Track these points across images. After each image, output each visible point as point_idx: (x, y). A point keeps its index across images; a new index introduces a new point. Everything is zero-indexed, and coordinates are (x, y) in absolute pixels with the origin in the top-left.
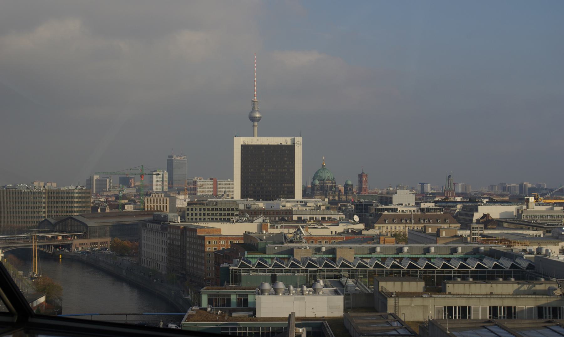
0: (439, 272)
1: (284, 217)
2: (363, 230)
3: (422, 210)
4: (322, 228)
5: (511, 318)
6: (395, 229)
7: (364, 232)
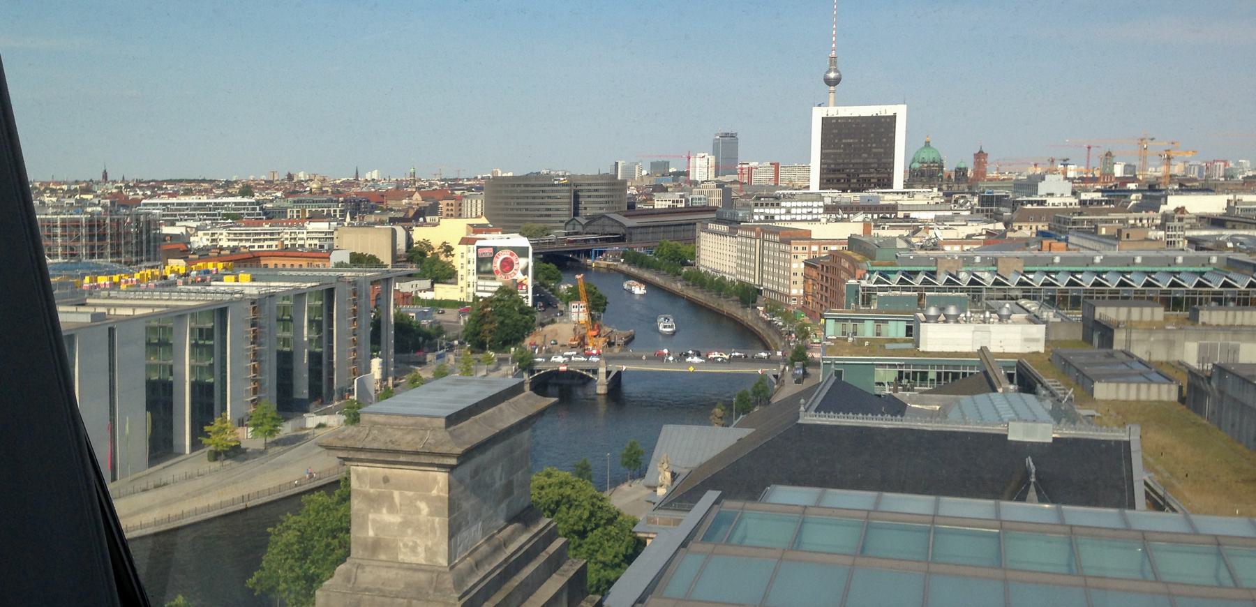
0: (1061, 291)
1: (887, 213)
3: (1083, 203)
5: (590, 379)
7: (1010, 234)
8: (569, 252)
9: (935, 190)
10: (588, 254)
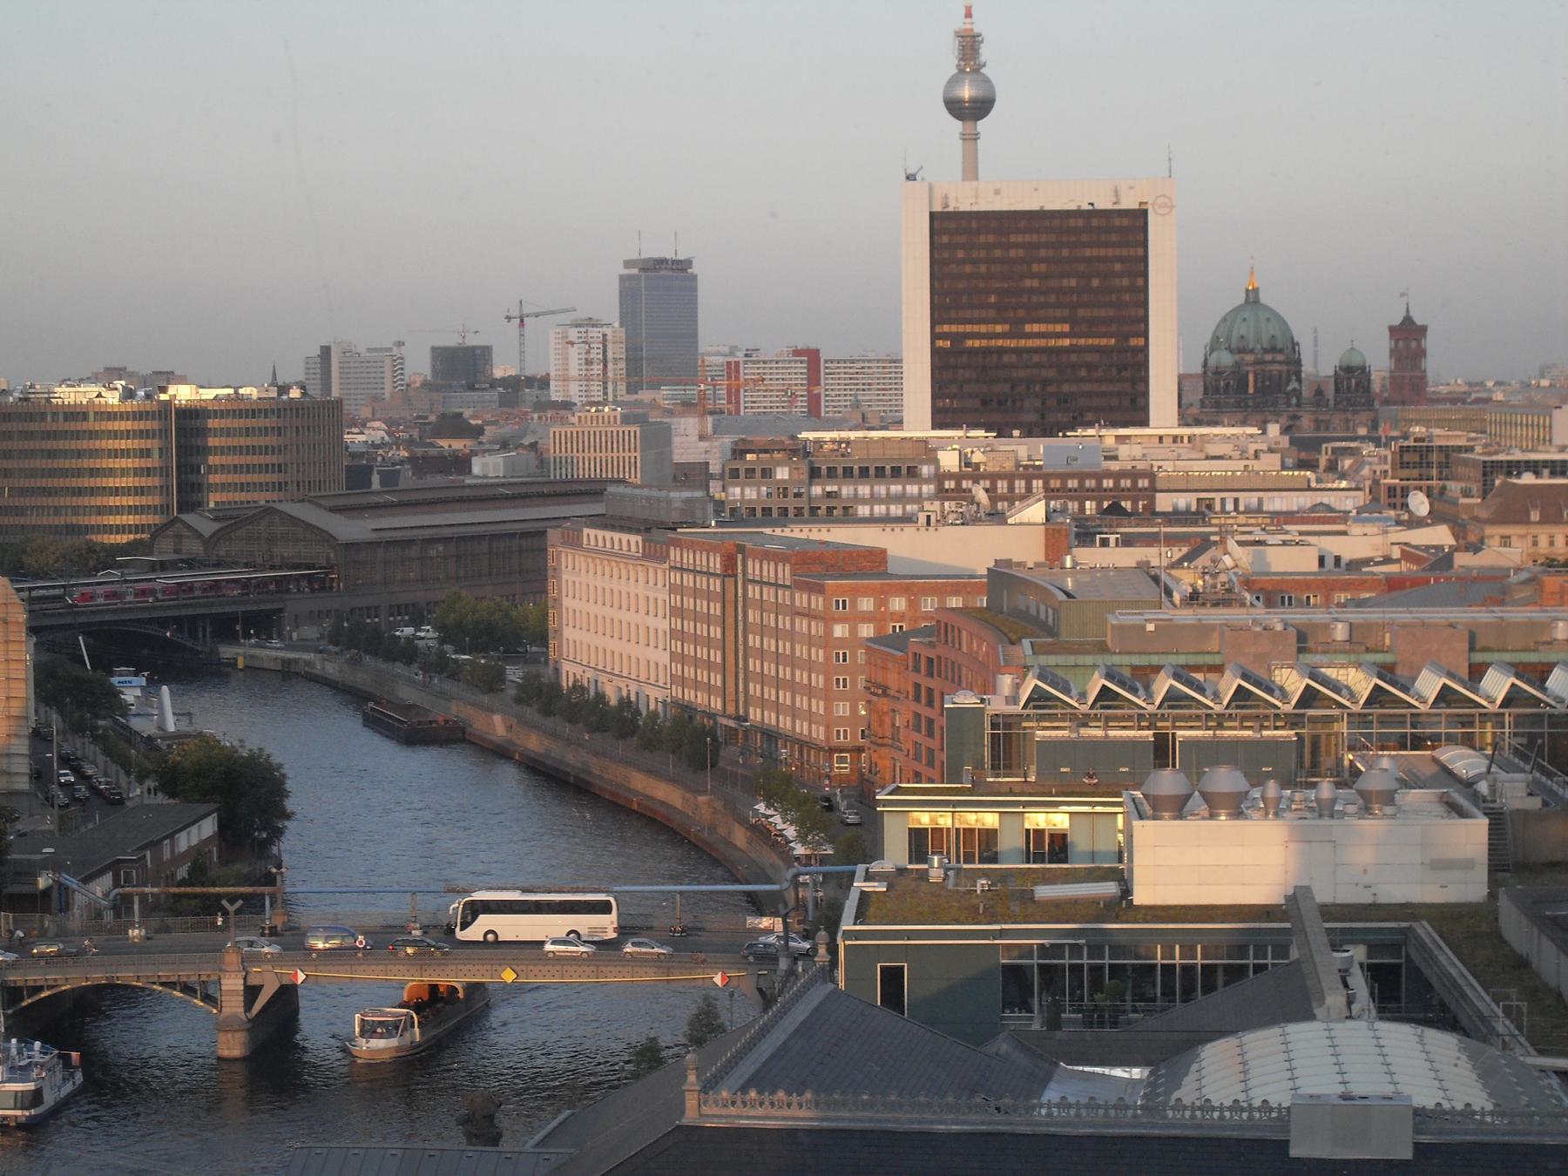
1: (1120, 505)
2: (1454, 549)
4: (1285, 543)
6: (1552, 543)
7: (1462, 560)
8: (163, 623)
9: (1274, 429)
10: (226, 628)
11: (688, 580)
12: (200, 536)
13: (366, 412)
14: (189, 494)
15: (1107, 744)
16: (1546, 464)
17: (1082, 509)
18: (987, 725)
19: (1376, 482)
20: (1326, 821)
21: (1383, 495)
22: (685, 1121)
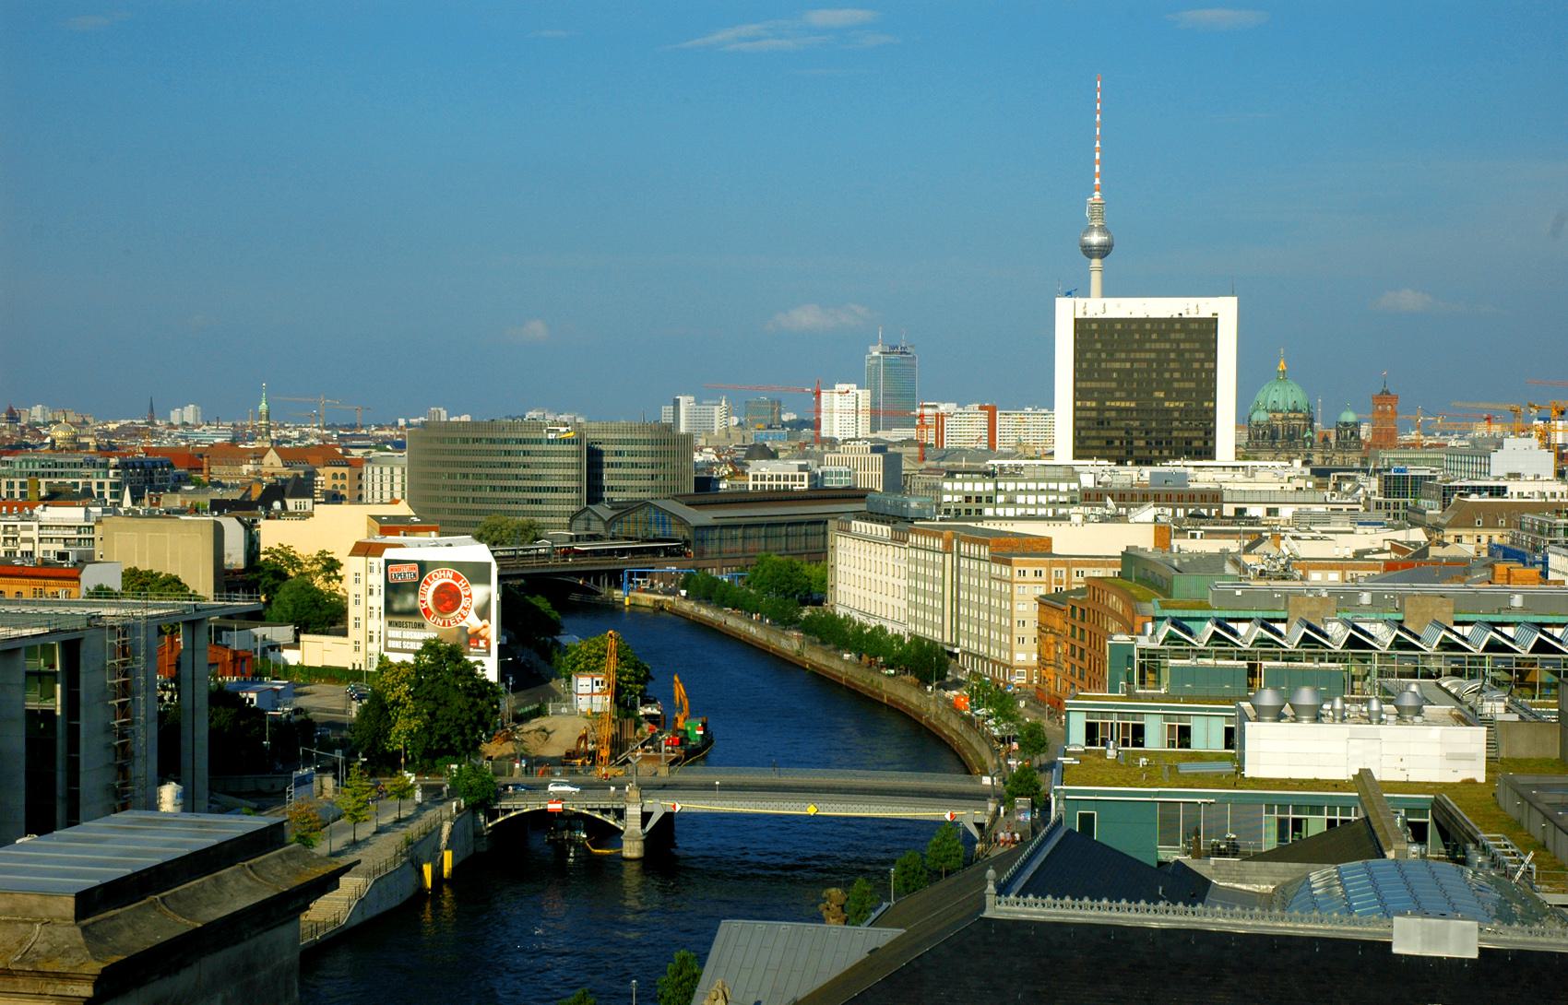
1: (1202, 507)
7: (1435, 551)
9: (1298, 463)
11: (921, 555)
12: (601, 519)
13: (702, 442)
14: (594, 491)
15: (1216, 669)
16: (1486, 488)
17: (1174, 513)
18: (1137, 658)
19: (1368, 499)
20: (1375, 726)
21: (1373, 506)
22: (986, 914)
